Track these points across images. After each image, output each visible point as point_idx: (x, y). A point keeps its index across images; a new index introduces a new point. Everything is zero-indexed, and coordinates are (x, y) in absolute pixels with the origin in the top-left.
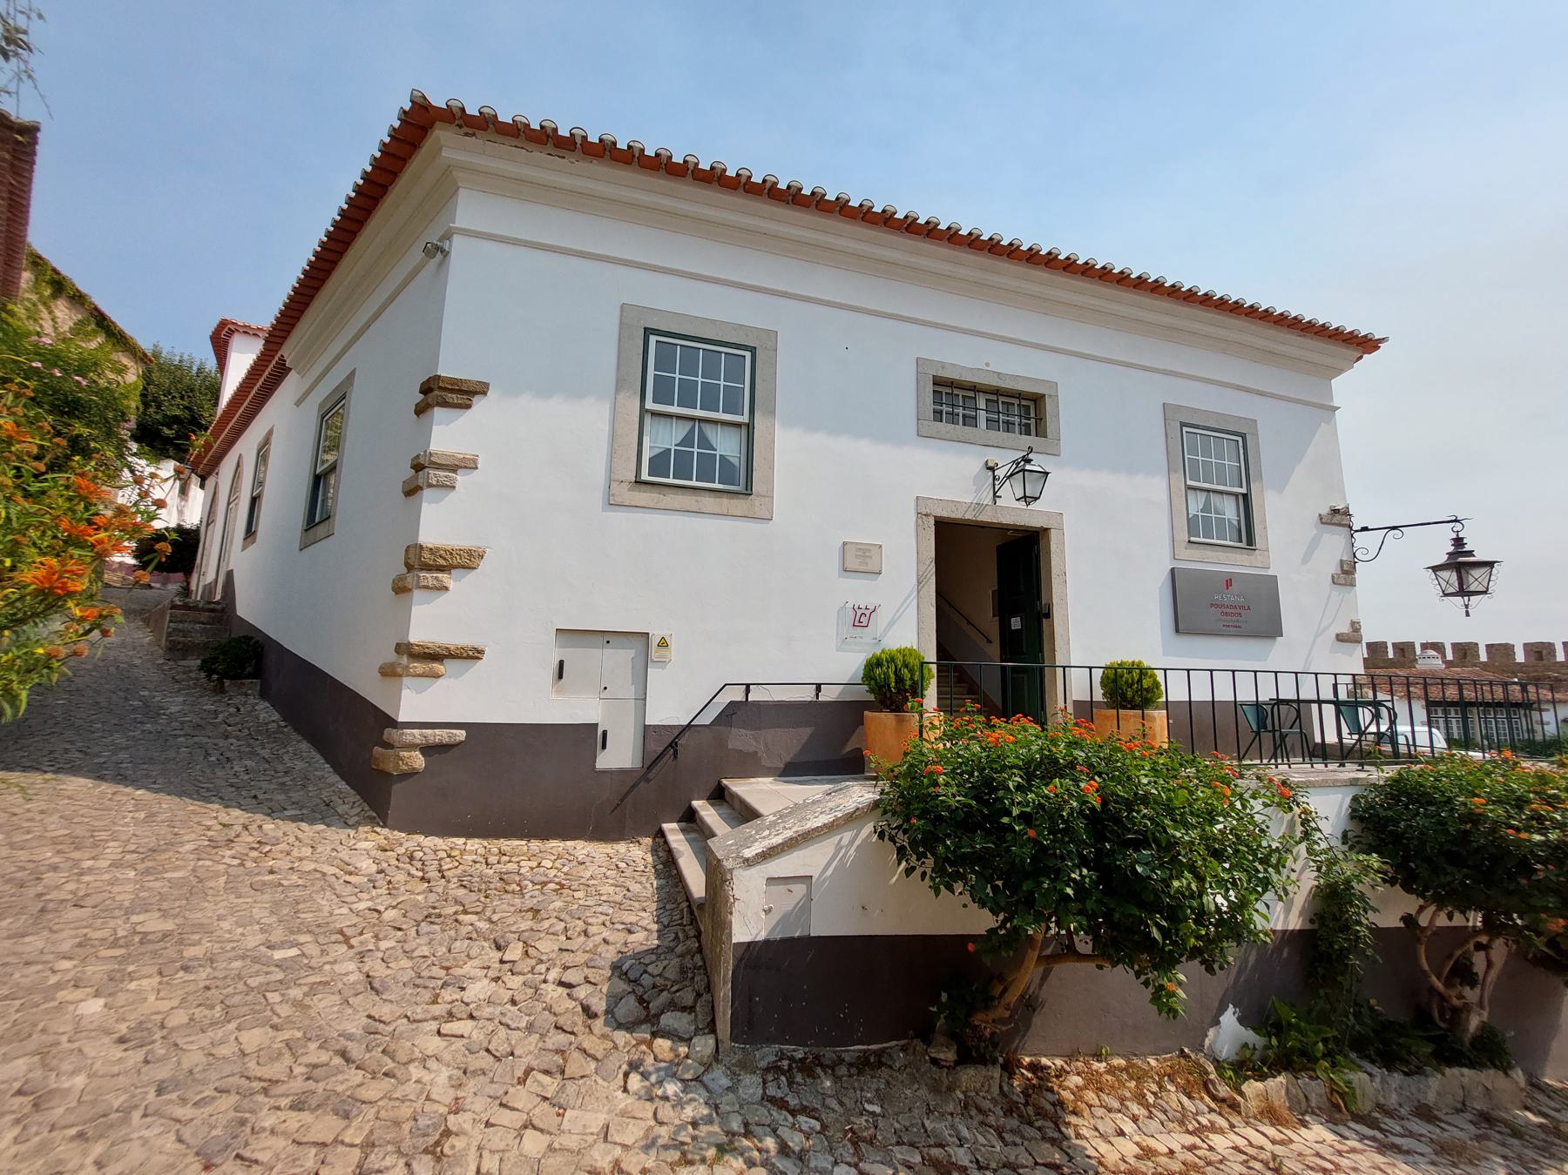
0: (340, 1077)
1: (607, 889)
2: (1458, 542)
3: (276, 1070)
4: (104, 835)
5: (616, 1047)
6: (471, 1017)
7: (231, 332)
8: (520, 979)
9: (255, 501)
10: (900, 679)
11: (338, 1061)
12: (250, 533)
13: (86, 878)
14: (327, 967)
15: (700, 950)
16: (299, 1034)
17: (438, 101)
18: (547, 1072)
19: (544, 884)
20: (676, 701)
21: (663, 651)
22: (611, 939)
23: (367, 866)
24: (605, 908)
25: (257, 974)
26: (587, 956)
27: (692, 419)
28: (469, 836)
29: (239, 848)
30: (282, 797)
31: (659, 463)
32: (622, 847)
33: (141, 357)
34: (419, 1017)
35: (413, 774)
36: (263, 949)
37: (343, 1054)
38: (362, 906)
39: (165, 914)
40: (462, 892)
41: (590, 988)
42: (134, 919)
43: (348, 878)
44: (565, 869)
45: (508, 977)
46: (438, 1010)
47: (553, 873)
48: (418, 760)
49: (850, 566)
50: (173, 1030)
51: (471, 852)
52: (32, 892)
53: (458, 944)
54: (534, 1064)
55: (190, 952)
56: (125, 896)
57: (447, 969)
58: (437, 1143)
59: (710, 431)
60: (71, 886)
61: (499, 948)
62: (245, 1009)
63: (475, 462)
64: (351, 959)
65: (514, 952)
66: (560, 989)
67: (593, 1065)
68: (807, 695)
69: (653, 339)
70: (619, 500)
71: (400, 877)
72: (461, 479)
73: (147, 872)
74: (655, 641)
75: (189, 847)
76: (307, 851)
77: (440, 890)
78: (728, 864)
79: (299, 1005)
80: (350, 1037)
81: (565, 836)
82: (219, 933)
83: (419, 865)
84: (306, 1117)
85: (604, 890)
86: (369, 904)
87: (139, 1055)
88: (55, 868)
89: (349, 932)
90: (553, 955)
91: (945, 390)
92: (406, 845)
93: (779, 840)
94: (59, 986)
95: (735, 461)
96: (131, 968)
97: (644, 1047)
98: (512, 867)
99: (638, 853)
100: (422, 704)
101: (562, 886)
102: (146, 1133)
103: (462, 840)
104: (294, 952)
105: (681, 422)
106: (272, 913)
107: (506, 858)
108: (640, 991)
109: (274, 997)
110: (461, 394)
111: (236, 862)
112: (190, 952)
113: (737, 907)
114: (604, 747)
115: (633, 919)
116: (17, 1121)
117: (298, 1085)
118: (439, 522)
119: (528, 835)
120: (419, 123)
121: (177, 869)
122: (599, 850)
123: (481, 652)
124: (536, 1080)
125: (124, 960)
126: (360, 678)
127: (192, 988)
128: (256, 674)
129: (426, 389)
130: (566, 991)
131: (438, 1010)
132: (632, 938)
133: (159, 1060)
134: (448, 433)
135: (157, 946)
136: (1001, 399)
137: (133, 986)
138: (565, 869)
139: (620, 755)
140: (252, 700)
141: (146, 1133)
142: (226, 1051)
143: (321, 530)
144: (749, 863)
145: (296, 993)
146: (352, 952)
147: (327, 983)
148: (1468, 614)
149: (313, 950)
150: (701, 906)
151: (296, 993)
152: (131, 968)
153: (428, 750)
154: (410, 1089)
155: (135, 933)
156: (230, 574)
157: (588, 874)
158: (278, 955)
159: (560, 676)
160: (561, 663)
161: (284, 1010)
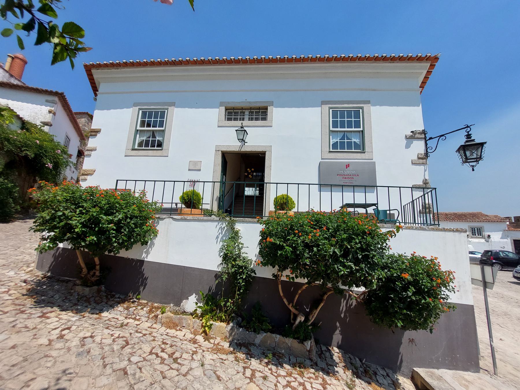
2: (469, 136)
27: (345, 131)
31: (335, 146)
59: (349, 135)
69: (331, 110)
72: (93, 153)
95: (358, 143)
136: (261, 111)
148: (473, 170)
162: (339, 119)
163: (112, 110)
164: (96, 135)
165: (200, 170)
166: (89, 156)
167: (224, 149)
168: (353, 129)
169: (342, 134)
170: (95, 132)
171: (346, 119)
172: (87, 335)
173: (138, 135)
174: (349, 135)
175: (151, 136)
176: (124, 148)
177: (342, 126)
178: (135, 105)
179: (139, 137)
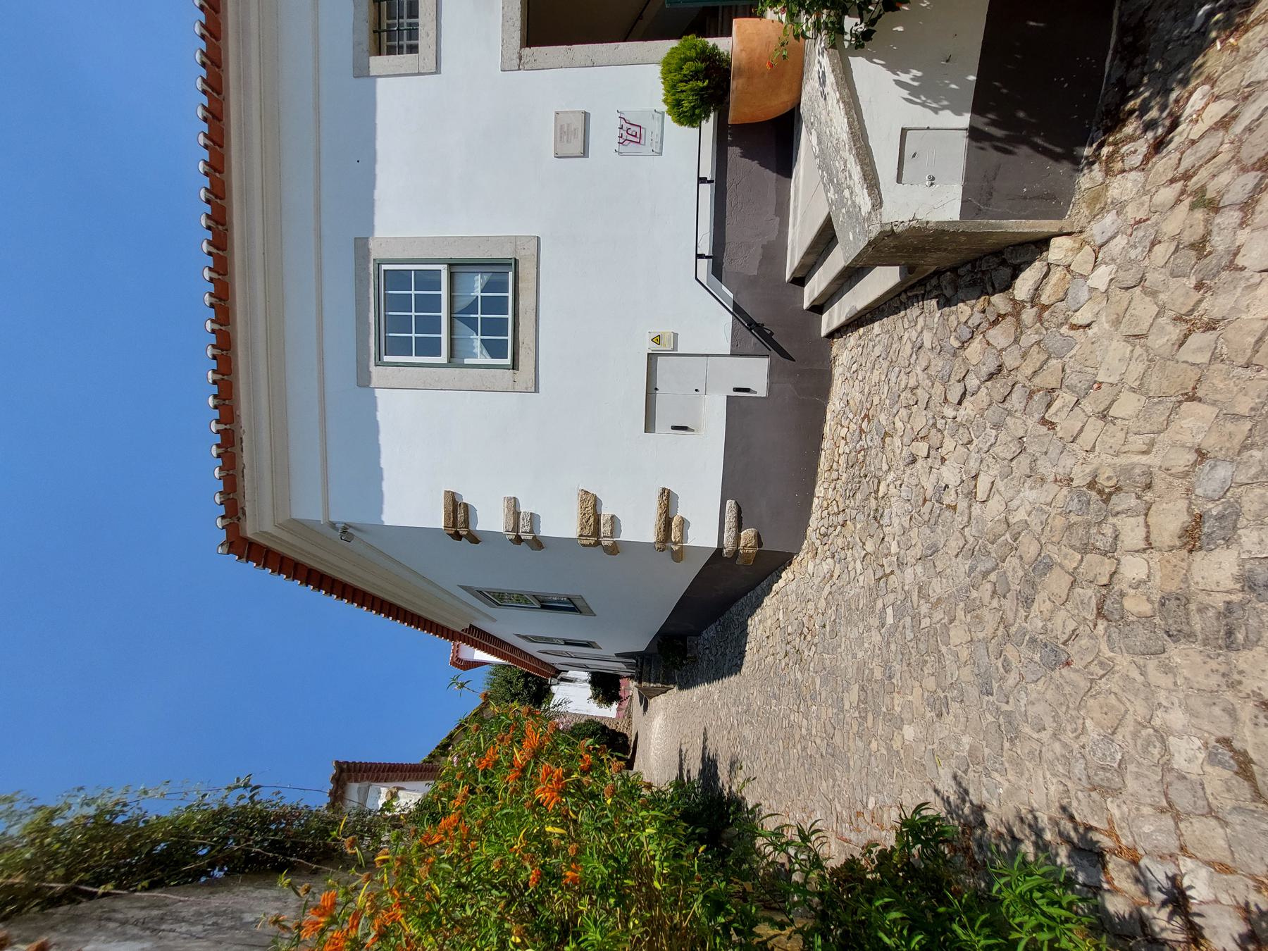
0: (1010, 574)
1: (875, 376)
3: (990, 619)
4: (785, 722)
5: (1038, 343)
6: (976, 477)
7: (458, 659)
8: (947, 441)
9: (567, 643)
10: (695, 76)
11: (993, 577)
12: (588, 645)
13: (814, 732)
14: (906, 588)
15: (954, 270)
16: (962, 605)
17: (223, 536)
18: (1049, 406)
19: (862, 431)
20: (713, 326)
21: (664, 340)
22: (924, 364)
23: (827, 565)
24: (893, 377)
25: (903, 635)
26: (937, 384)
28: (812, 495)
29: (804, 646)
30: (769, 622)
31: (495, 349)
32: (837, 371)
33: (486, 704)
34: (966, 519)
35: (758, 537)
36: (883, 631)
37: (985, 574)
38: (859, 567)
39: (847, 689)
40: (858, 496)
41: (971, 376)
42: (847, 707)
43: (836, 576)
44: (851, 416)
45: (943, 451)
46: (962, 505)
47: (853, 426)
48: (747, 534)
49: (580, 150)
50: (938, 686)
51: (826, 493)
52: (819, 760)
53: (903, 494)
54: (1037, 416)
55: (878, 674)
56: (828, 713)
57: (925, 500)
58: (1100, 492)
59: (461, 304)
60: (818, 741)
61: (914, 461)
62: (932, 641)
63: (509, 499)
64: (903, 572)
65: (921, 448)
66: (965, 403)
67: (1053, 362)
68: (707, 190)
70: (531, 384)
71: (840, 541)
73: (813, 699)
74: (655, 347)
75: (799, 675)
76: (811, 605)
77: (854, 512)
78: (875, 231)
79: (935, 606)
80: (972, 569)
81: (823, 420)
82: (866, 657)
83: (831, 529)
84: (1041, 597)
85: (875, 378)
86: (858, 562)
87: (954, 706)
88: (804, 749)
89: (879, 574)
90: (930, 415)
91: (385, 43)
92: (814, 538)
93: (856, 171)
94: (889, 748)
95: (486, 277)
96: (884, 709)
97: (1046, 314)
98: (842, 460)
99: (844, 353)
100: (704, 530)
101: (866, 416)
102: (1023, 702)
103: (816, 501)
104: (889, 611)
105: (456, 330)
106: (856, 625)
107: (835, 466)
108: (985, 325)
109: (925, 623)
110: (458, 511)
111: (813, 648)
112: (878, 674)
113: (923, 216)
114: (747, 390)
115: (909, 345)
116: (988, 775)
117: (1008, 604)
118: (561, 523)
119: (817, 450)
120: (244, 547)
121: (814, 683)
122: (838, 389)
123: (664, 490)
124: (1056, 414)
125: (876, 714)
126: (682, 578)
127: (907, 675)
128: (683, 638)
129: (457, 536)
130: (968, 397)
131: (962, 505)
132: (927, 344)
133: (962, 695)
134: (491, 520)
135: (870, 694)
137: (898, 709)
138: (851, 416)
139: (755, 374)
140: (701, 641)
141: (1023, 702)
142: (964, 654)
143: (578, 603)
144: (878, 203)
145: (924, 609)
146: (897, 571)
147: (920, 588)
149: (890, 598)
150: (908, 270)
151: (924, 609)
152: (884, 709)
153: (739, 526)
154: (1035, 522)
155: (858, 707)
156: (617, 655)
157: (858, 396)
158: (890, 620)
159: (685, 428)
160: (675, 428)
161: (938, 615)
162: (413, 335)
163: (384, 463)
164: (466, 505)
165: (586, 116)
166: (534, 518)
167: (516, 36)
168: (444, 292)
169: (460, 326)
170: (455, 511)
171: (413, 314)
172: (1098, 558)
173: (467, 361)
174: (461, 304)
175: (469, 309)
176: (510, 400)
177: (435, 325)
178: (364, 380)
179: (475, 356)
